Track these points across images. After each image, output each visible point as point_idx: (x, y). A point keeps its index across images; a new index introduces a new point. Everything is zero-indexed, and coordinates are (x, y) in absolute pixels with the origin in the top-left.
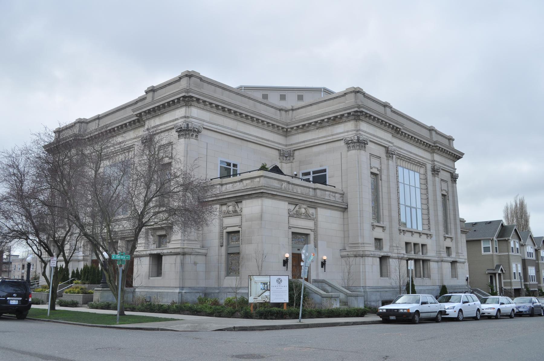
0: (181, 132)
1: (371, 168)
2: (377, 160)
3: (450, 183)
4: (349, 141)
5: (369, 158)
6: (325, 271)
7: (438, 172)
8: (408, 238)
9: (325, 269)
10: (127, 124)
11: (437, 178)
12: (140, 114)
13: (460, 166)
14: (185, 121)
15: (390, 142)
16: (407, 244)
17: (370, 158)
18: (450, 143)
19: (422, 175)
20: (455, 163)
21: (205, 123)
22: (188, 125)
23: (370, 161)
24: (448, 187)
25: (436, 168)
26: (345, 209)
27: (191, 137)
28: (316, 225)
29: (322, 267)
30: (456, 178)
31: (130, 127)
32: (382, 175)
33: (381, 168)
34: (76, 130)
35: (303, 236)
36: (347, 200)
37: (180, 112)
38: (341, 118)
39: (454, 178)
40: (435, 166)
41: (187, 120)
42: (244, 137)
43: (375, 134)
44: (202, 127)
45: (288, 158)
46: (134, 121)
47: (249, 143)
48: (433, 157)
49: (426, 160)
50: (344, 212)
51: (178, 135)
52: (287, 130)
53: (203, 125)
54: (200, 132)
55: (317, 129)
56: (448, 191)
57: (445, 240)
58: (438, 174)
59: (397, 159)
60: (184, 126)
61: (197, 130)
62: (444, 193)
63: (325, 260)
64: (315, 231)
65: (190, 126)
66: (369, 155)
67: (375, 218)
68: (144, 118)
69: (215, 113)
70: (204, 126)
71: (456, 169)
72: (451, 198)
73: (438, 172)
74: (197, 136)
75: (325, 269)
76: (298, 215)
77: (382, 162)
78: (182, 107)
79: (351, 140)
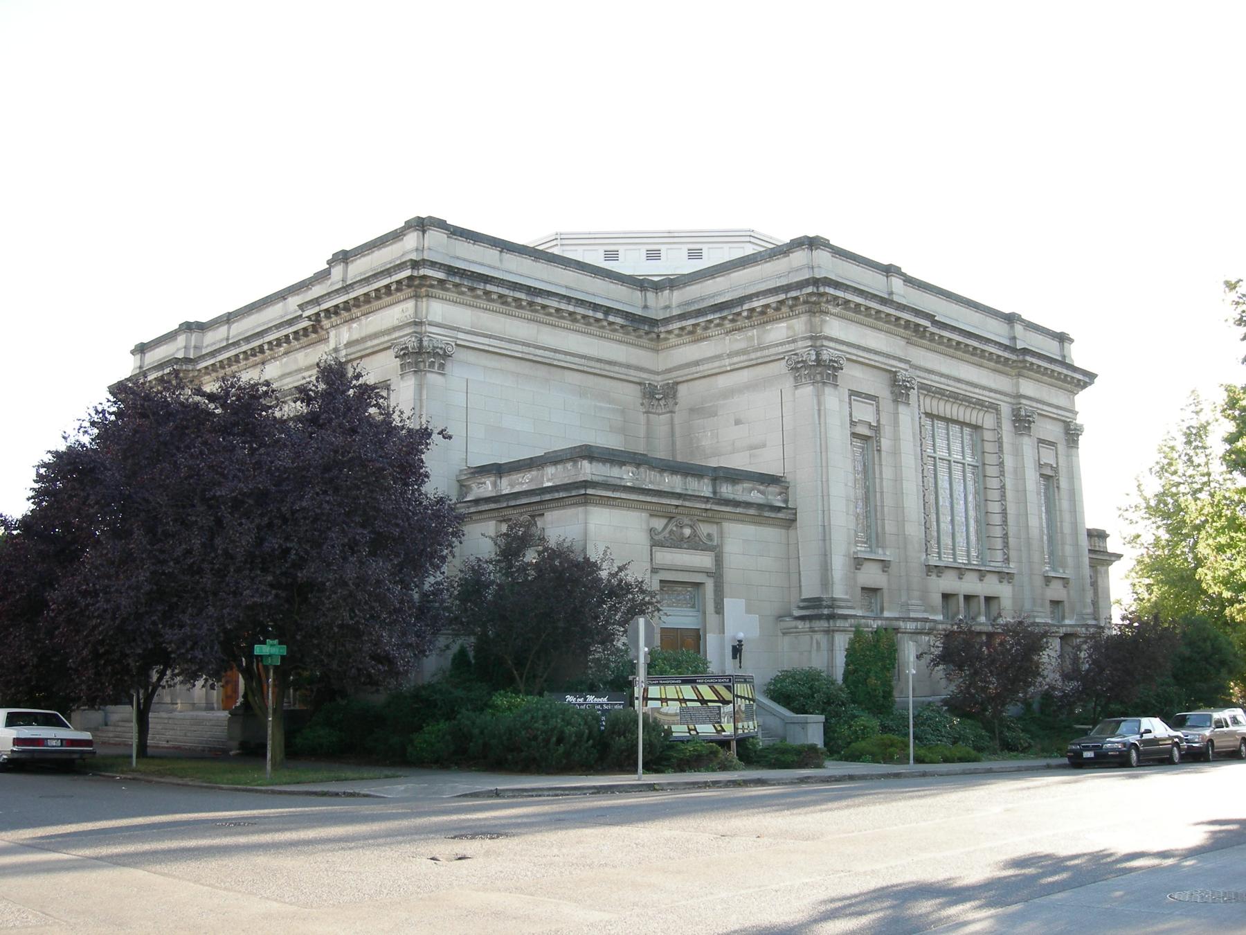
0: (407, 357)
1: (853, 423)
2: (870, 404)
3: (1061, 448)
4: (799, 362)
5: (847, 400)
6: (740, 667)
7: (1030, 422)
8: (948, 583)
9: (740, 662)
10: (291, 337)
11: (1026, 440)
12: (318, 314)
13: (1085, 404)
14: (416, 332)
15: (900, 360)
16: (946, 597)
17: (850, 400)
18: (1062, 349)
19: (990, 432)
20: (1076, 397)
21: (461, 335)
22: (421, 341)
23: (851, 408)
24: (1057, 457)
25: (1023, 413)
26: (791, 522)
27: (429, 367)
28: (719, 561)
29: (734, 657)
30: (1078, 435)
31: (296, 343)
32: (882, 439)
33: (878, 421)
34: (175, 349)
35: (689, 589)
36: (795, 501)
37: (397, 313)
38: (777, 309)
39: (1072, 434)
40: (1021, 408)
41: (418, 329)
42: (555, 359)
43: (863, 343)
44: (453, 344)
45: (662, 402)
46: (305, 329)
47: (567, 373)
48: (1017, 385)
49: (998, 396)
50: (788, 528)
51: (401, 365)
52: (658, 336)
53: (457, 338)
54: (449, 356)
55: (727, 333)
56: (1058, 466)
57: (1047, 585)
58: (1029, 428)
59: (922, 398)
60: (412, 343)
61: (441, 352)
62: (1049, 472)
63: (740, 641)
64: (717, 574)
65: (425, 344)
66: (847, 393)
67: (865, 540)
68: (326, 323)
69: (483, 308)
70: (459, 342)
71: (1077, 413)
72: (1064, 484)
73: (1030, 422)
74: (442, 366)
75: (740, 662)
76: (677, 542)
77: (881, 409)
78: (408, 301)
79: (802, 361)
